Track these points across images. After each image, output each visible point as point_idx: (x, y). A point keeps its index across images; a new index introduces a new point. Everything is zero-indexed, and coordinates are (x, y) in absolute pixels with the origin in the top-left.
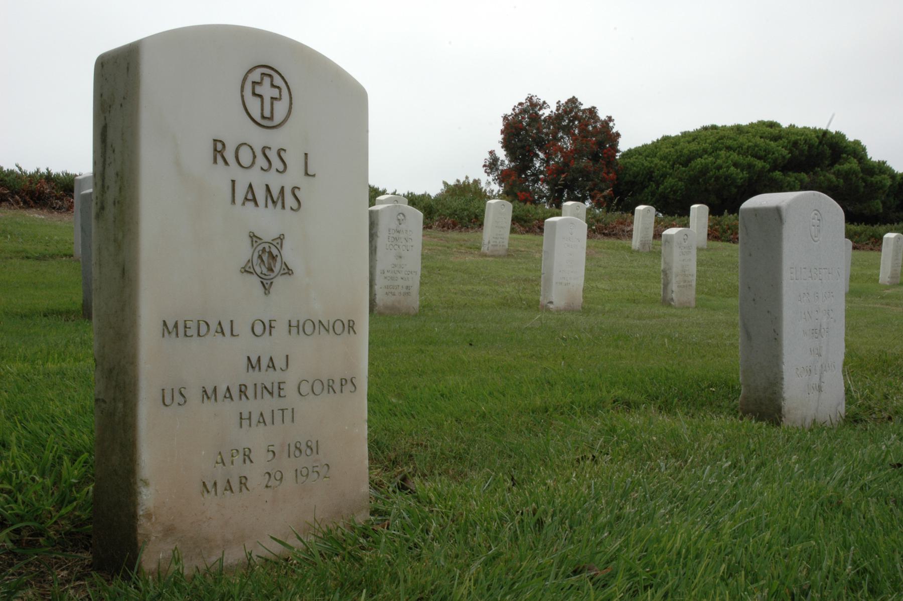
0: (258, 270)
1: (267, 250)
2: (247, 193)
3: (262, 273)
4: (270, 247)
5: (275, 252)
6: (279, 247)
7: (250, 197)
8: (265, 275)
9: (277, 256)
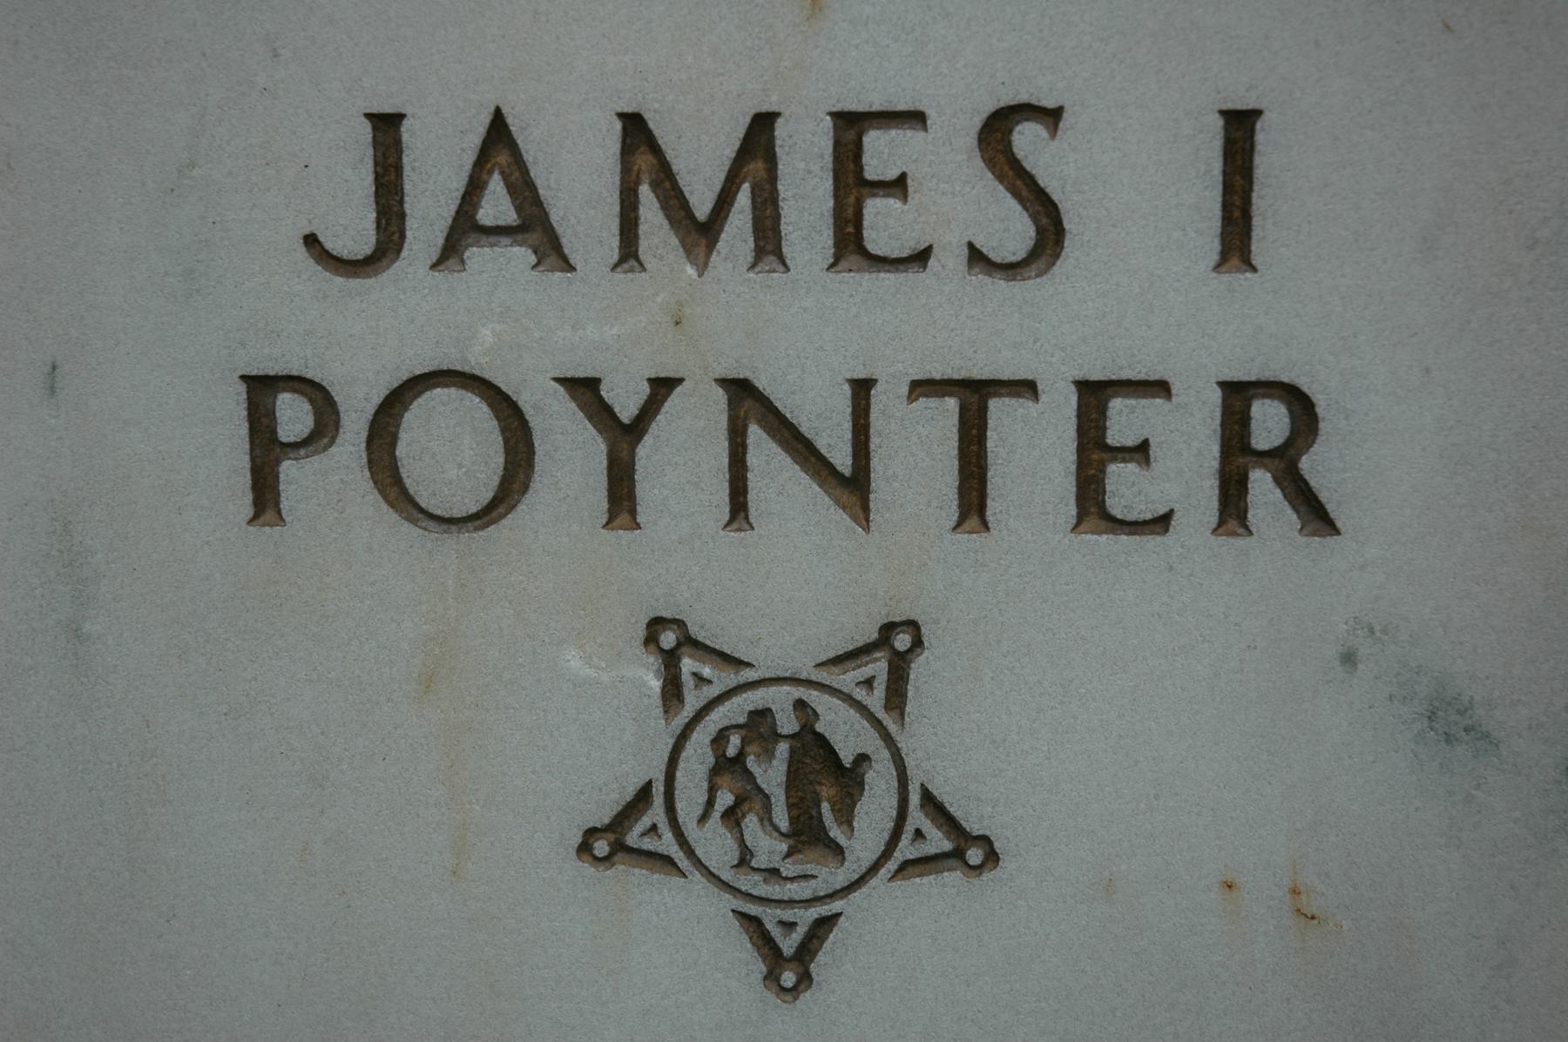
1: (788, 723)
2: (474, 189)
3: (744, 860)
6: (906, 850)
8: (774, 873)
9: (862, 758)
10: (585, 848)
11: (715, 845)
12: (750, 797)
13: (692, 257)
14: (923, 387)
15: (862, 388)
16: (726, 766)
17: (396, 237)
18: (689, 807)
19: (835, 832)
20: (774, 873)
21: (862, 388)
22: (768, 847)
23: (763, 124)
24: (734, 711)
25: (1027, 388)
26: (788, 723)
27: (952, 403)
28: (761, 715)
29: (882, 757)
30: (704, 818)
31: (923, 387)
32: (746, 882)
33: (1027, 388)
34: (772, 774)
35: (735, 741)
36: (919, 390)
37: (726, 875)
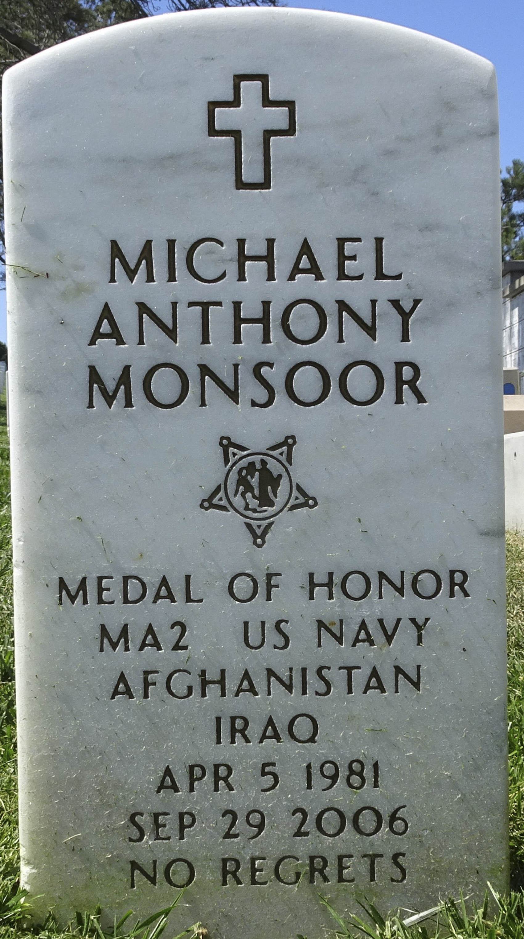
0: (238, 501)
1: (258, 466)
3: (247, 508)
4: (263, 462)
5: (274, 467)
7: (105, 327)
10: (202, 506)
11: (238, 501)
12: (249, 488)
13: (276, 4)
14: (191, 304)
15: (174, 305)
16: (242, 481)
17: (231, 396)
18: (231, 491)
19: (271, 495)
20: (255, 511)
21: (174, 305)
22: (254, 503)
23: (84, 579)
24: (244, 463)
25: (219, 304)
26: (258, 466)
27: (408, 311)
28: (252, 464)
29: (285, 474)
30: (235, 495)
31: (191, 304)
32: (249, 513)
33: (219, 304)
34: (254, 481)
35: (244, 473)
36: (190, 305)
37: (241, 510)
